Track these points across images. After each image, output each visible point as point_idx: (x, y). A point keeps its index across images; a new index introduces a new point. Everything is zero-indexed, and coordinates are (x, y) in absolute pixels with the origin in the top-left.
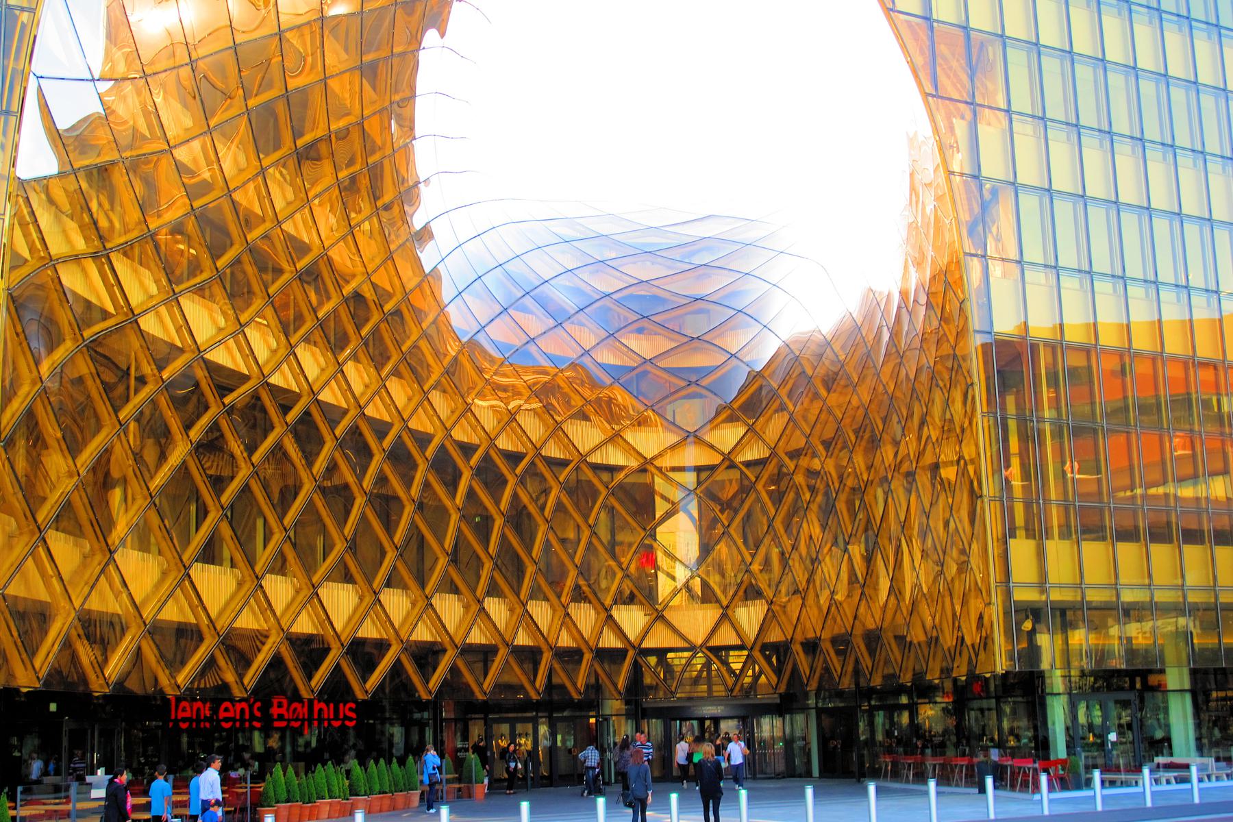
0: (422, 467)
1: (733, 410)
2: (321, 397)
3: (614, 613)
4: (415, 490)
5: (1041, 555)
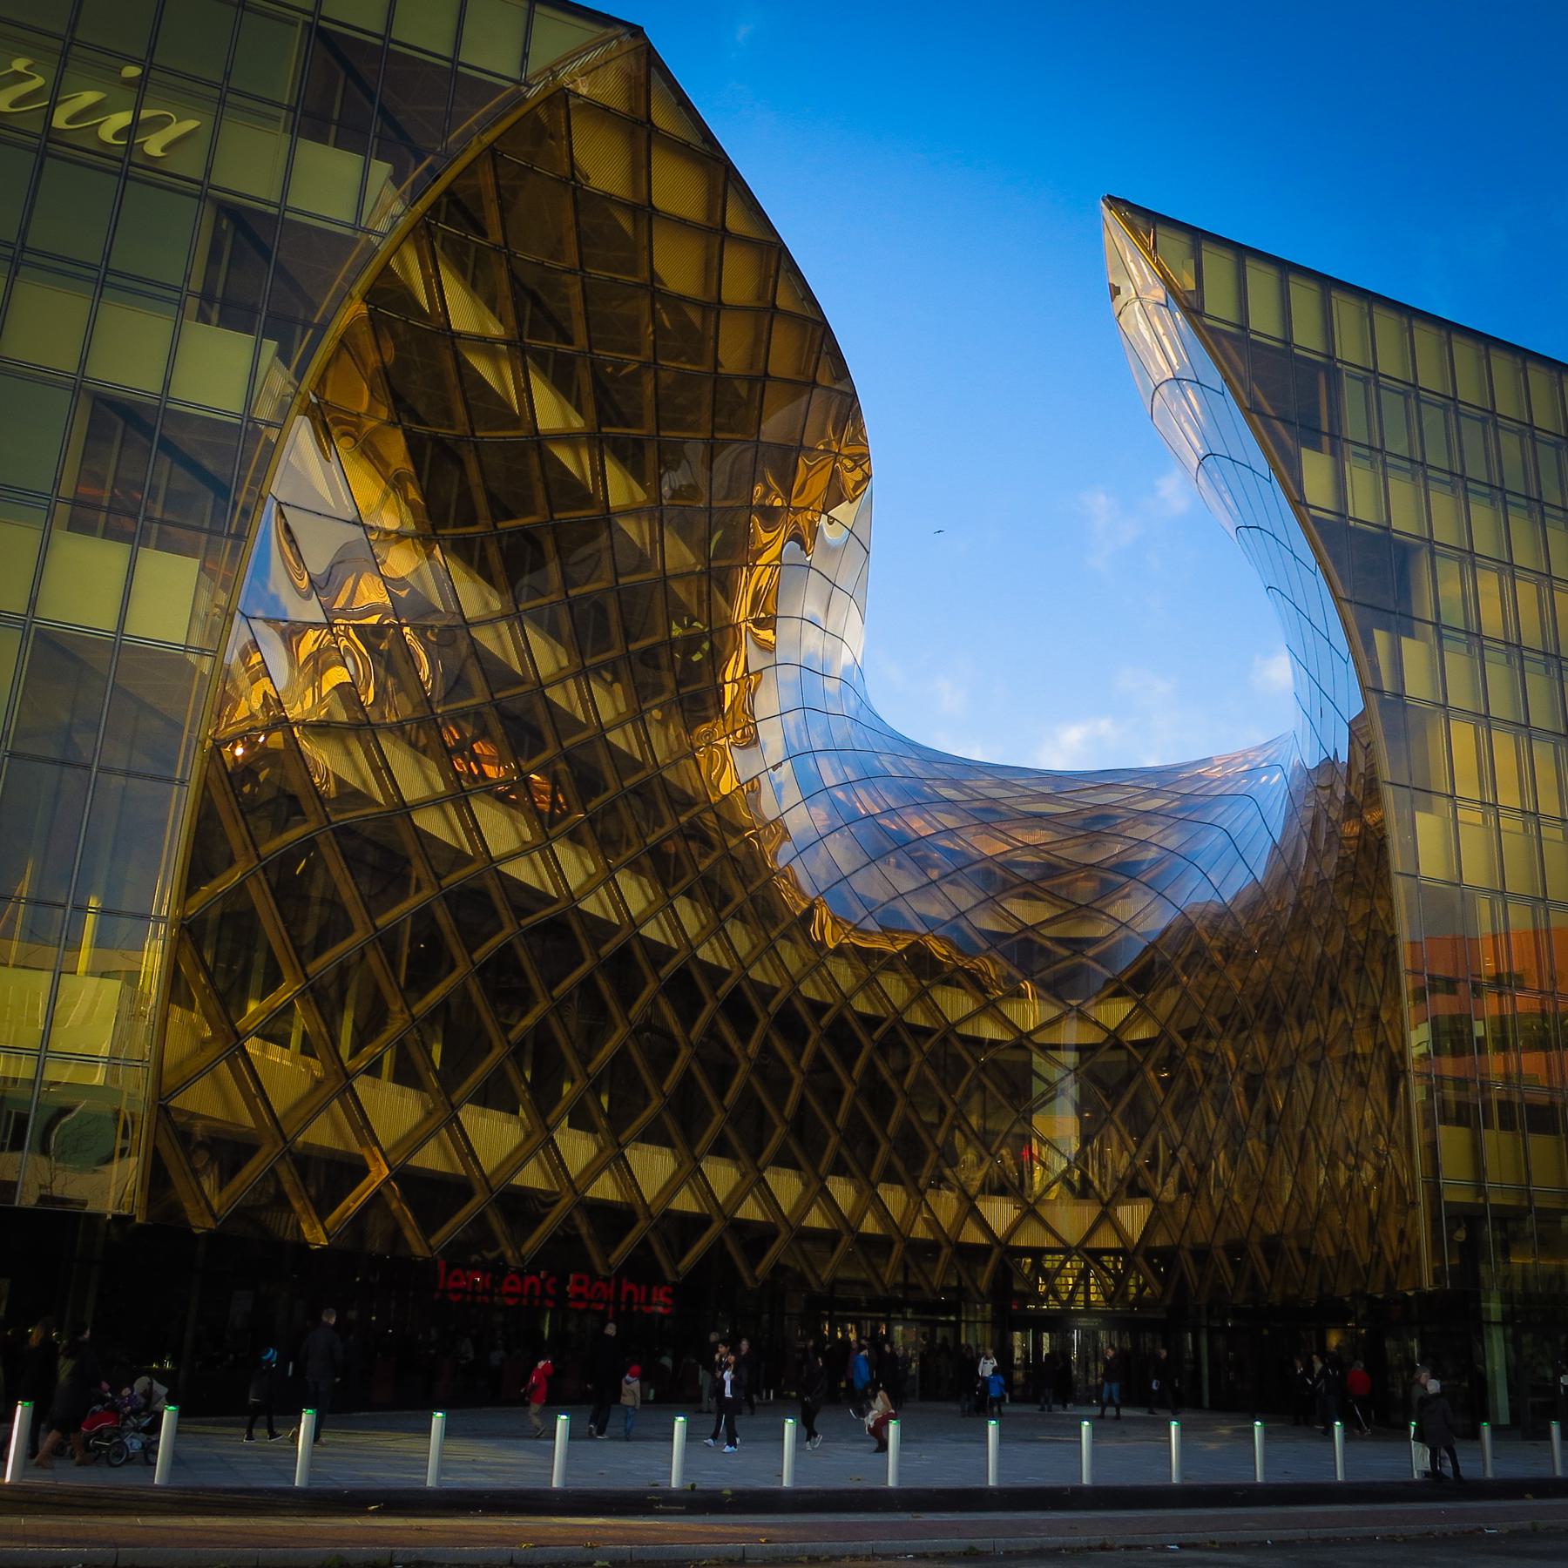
0: (763, 1022)
1: (1121, 982)
2: (642, 932)
3: (980, 1205)
4: (753, 1047)
5: (1476, 1150)
